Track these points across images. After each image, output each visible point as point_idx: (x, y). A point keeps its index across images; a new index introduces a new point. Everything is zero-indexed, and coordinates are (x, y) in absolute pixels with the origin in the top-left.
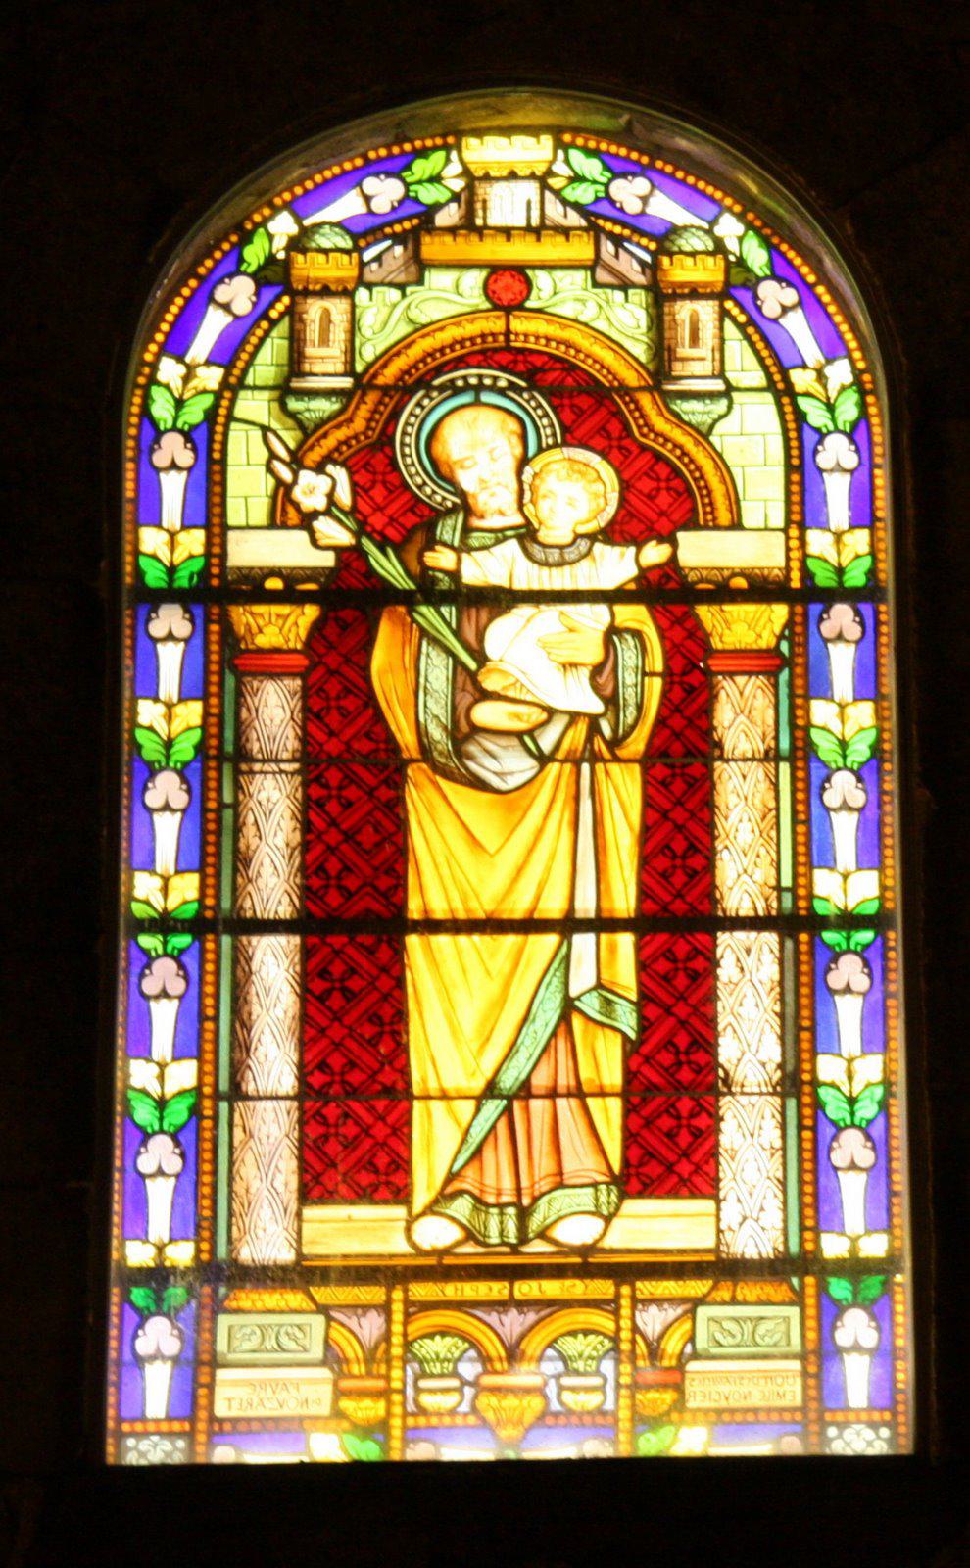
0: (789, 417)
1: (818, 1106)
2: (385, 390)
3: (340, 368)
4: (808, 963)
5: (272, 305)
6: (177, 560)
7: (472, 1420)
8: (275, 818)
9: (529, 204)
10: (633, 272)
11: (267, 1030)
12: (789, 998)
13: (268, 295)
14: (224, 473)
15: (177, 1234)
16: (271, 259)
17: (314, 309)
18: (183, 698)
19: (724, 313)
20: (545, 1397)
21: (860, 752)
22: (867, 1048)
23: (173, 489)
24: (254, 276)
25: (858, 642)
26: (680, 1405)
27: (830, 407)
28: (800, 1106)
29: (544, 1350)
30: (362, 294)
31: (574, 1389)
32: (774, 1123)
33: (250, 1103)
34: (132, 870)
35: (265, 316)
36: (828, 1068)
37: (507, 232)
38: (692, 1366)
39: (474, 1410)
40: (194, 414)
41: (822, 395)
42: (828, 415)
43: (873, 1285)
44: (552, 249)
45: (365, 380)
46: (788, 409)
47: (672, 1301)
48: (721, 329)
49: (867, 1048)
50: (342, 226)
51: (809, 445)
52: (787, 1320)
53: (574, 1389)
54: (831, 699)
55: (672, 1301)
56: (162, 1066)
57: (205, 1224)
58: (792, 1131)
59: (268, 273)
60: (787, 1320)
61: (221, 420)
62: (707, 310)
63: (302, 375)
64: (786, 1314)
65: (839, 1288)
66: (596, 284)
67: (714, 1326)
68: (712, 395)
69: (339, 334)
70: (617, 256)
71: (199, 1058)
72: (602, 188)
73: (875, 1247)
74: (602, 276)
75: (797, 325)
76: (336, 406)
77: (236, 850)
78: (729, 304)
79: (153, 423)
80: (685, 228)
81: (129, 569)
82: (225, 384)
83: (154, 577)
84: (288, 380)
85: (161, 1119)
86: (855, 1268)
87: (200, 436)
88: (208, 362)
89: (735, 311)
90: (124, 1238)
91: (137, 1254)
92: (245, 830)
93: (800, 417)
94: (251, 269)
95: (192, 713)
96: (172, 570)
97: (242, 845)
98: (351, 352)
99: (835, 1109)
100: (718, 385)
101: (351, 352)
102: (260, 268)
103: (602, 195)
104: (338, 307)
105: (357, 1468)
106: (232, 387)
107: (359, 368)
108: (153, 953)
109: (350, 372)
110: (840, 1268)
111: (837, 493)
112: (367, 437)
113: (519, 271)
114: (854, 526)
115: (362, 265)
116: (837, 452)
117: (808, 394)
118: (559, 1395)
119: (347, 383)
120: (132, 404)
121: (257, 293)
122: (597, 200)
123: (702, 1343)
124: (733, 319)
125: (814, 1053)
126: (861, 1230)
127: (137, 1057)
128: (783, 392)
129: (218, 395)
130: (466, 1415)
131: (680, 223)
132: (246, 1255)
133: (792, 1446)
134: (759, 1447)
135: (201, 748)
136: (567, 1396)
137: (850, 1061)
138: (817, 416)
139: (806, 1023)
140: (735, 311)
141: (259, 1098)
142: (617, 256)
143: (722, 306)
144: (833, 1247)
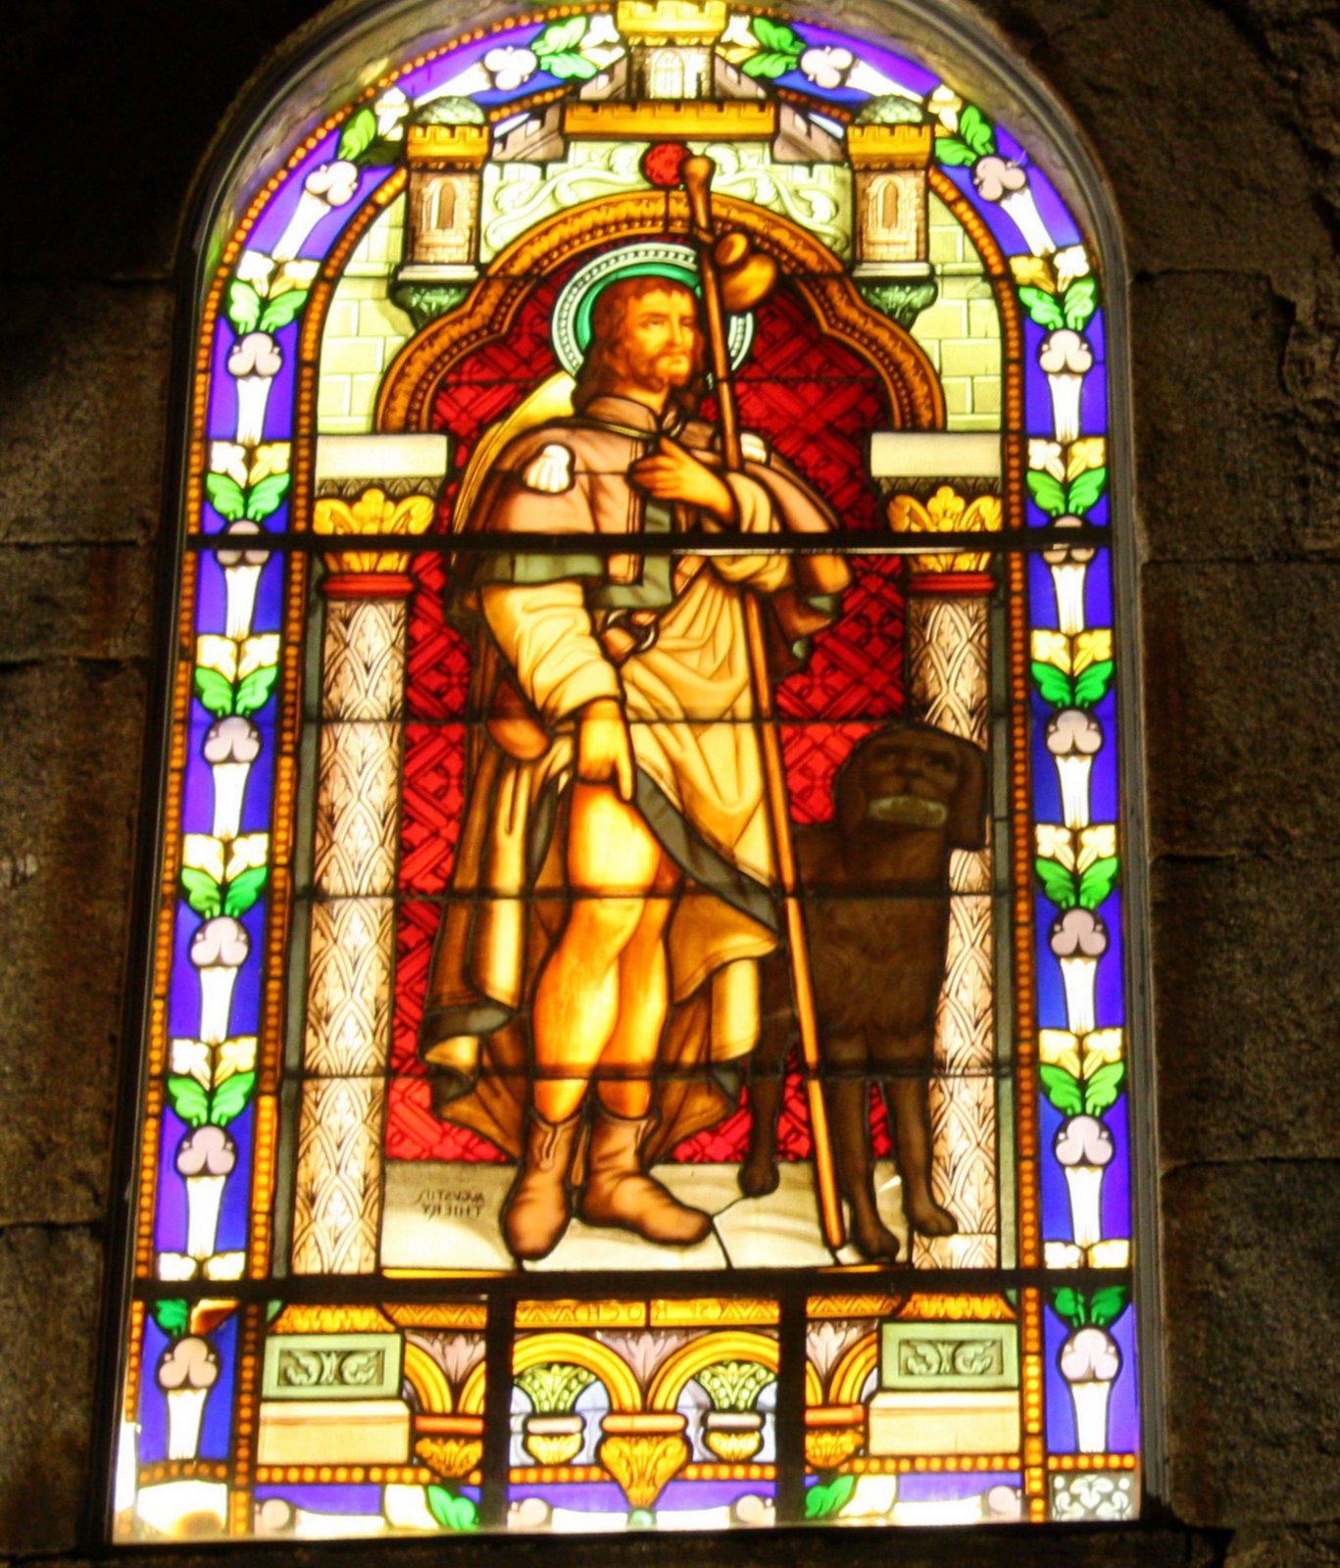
0: (1010, 314)
1: (1041, 1090)
2: (515, 279)
3: (462, 255)
4: (1029, 1001)
5: (380, 186)
6: (243, 671)
7: (595, 1473)
8: (371, 771)
9: (699, 76)
10: (822, 146)
11: (337, 1196)
12: (999, 669)
13: (371, 180)
14: (315, 379)
15: (222, 1246)
16: (378, 142)
17: (433, 188)
18: (268, 439)
19: (929, 187)
20: (687, 1441)
21: (1104, 1093)
22: (1103, 1021)
23: (252, 402)
24: (355, 162)
25: (1113, 1381)
26: (862, 1451)
27: (1059, 299)
28: (1016, 1090)
29: (699, 1131)
30: (491, 171)
31: (728, 1431)
32: (980, 1168)
33: (324, 1083)
34: (207, 441)
35: (369, 200)
36: (1054, 1045)
37: (677, 104)
38: (881, 1401)
39: (599, 1462)
40: (281, 315)
41: (1069, 865)
42: (1057, 309)
43: (1107, 1303)
44: (730, 121)
45: (492, 271)
46: (1008, 304)
47: (852, 1320)
48: (926, 207)
49: (1103, 1021)
50: (473, 99)
51: (1032, 343)
52: (998, 1343)
53: (728, 1431)
54: (1067, 1028)
55: (852, 1320)
56: (239, 644)
57: (250, 1347)
58: (1008, 1191)
59: (373, 158)
60: (998, 1343)
61: (301, 502)
62: (909, 185)
63: (413, 263)
64: (997, 1337)
65: (1066, 1301)
66: (774, 161)
67: (906, 1351)
68: (915, 282)
69: (463, 218)
70: (809, 134)
71: (283, 632)
72: (794, 60)
73: (1114, 1255)
74: (782, 150)
75: (1023, 211)
76: (456, 299)
77: (316, 806)
78: (936, 179)
79: (233, 326)
80: (884, 99)
81: (194, 493)
82: (320, 278)
83: (1053, 690)
84: (399, 268)
85: (210, 1109)
86: (1086, 1280)
87: (289, 340)
88: (298, 258)
89: (944, 187)
90: (181, 834)
91: (173, 1268)
92: (330, 785)
93: (1023, 311)
94: (352, 156)
95: (266, 649)
96: (224, 888)
97: (324, 800)
98: (476, 235)
99: (1063, 1095)
100: (921, 270)
101: (476, 235)
102: (362, 154)
103: (793, 67)
104: (463, 185)
105: (444, 1546)
106: (327, 281)
107: (485, 257)
108: (195, 1123)
109: (474, 260)
110: (1065, 1277)
111: (1066, 401)
112: (491, 332)
113: (680, 141)
114: (1085, 434)
115: (492, 141)
116: (1066, 353)
117: (1032, 285)
118: (705, 1440)
119: (469, 273)
120: (141, 1224)
121: (359, 180)
122: (788, 73)
123: (891, 1378)
124: (940, 196)
125: (1036, 1029)
126: (1079, 626)
127: (183, 1036)
128: (1001, 283)
129: (312, 292)
130: (586, 1466)
131: (877, 92)
132: (308, 1263)
133: (1007, 1507)
134: (959, 1511)
135: (277, 689)
136: (719, 1442)
137: (1081, 1038)
138: (1042, 311)
139: (1013, 369)
140: (944, 187)
141: (331, 1076)
142: (809, 134)
143: (927, 180)
144: (1059, 1257)
